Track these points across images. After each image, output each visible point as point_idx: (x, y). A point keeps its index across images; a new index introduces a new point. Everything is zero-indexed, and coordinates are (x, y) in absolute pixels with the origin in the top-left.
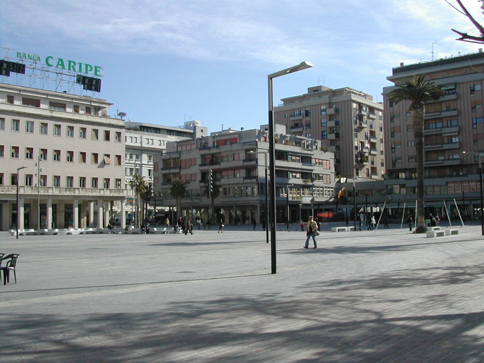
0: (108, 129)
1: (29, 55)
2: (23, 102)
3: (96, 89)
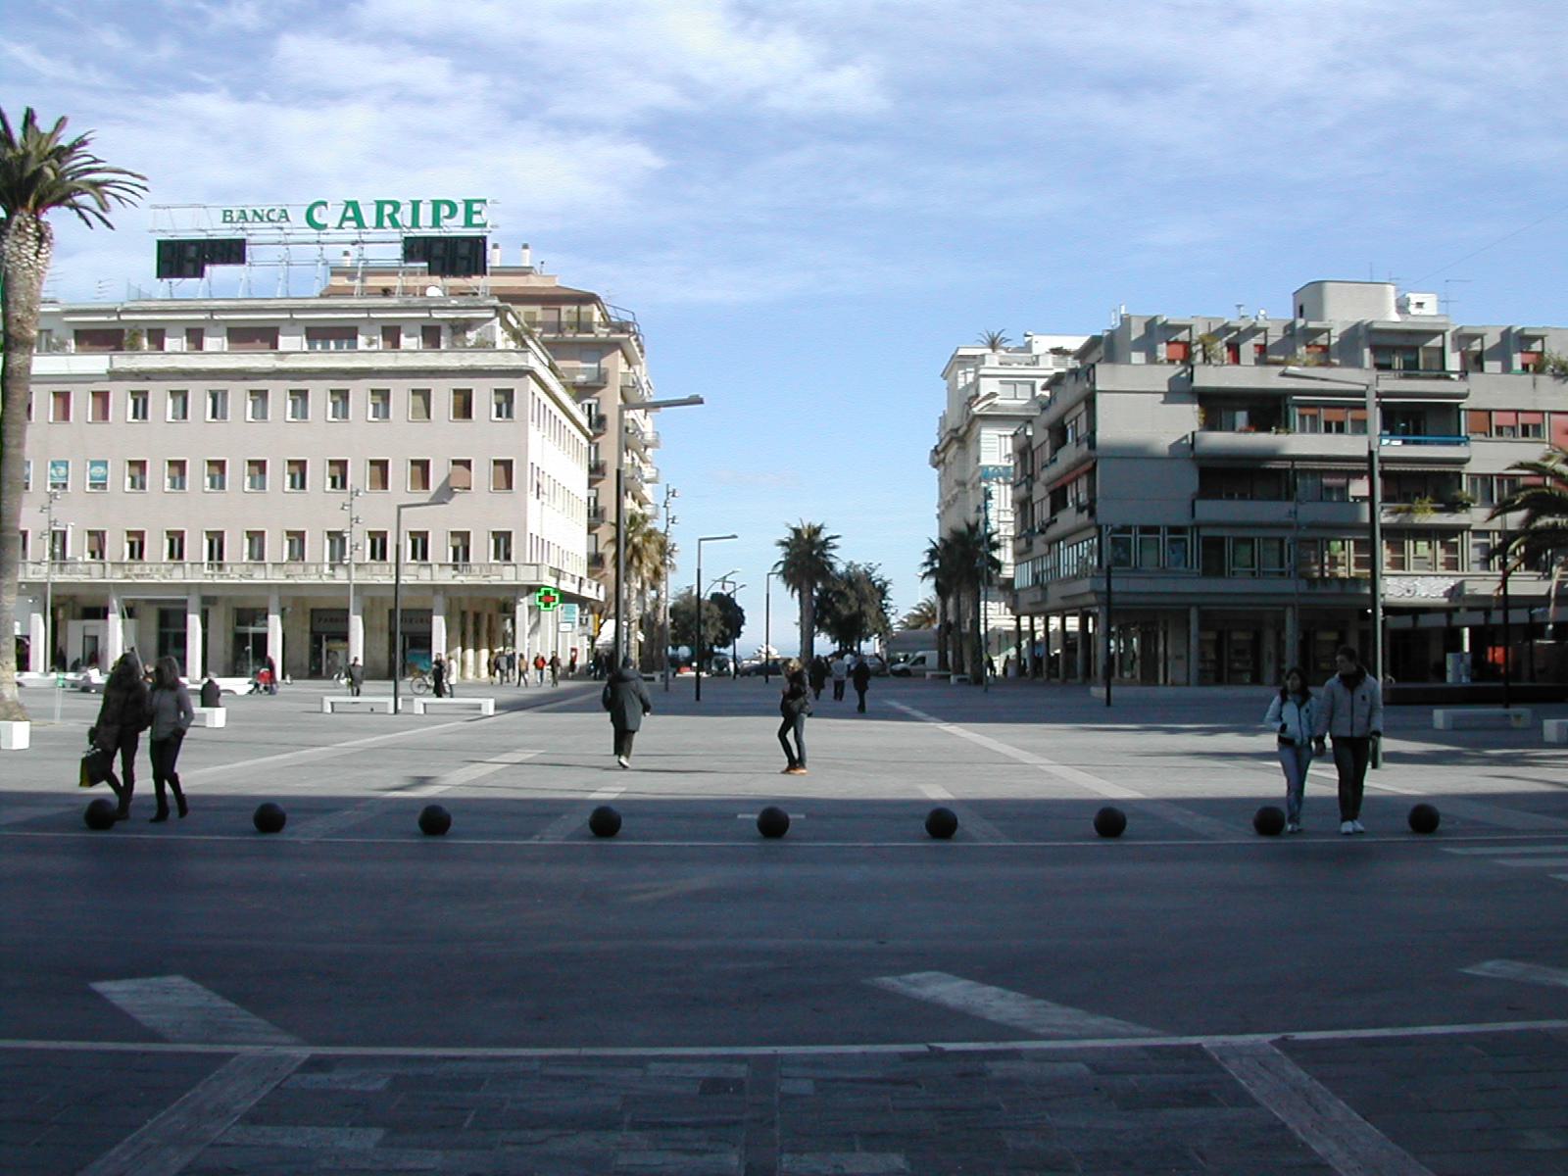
0: (463, 384)
1: (255, 212)
2: (424, 338)
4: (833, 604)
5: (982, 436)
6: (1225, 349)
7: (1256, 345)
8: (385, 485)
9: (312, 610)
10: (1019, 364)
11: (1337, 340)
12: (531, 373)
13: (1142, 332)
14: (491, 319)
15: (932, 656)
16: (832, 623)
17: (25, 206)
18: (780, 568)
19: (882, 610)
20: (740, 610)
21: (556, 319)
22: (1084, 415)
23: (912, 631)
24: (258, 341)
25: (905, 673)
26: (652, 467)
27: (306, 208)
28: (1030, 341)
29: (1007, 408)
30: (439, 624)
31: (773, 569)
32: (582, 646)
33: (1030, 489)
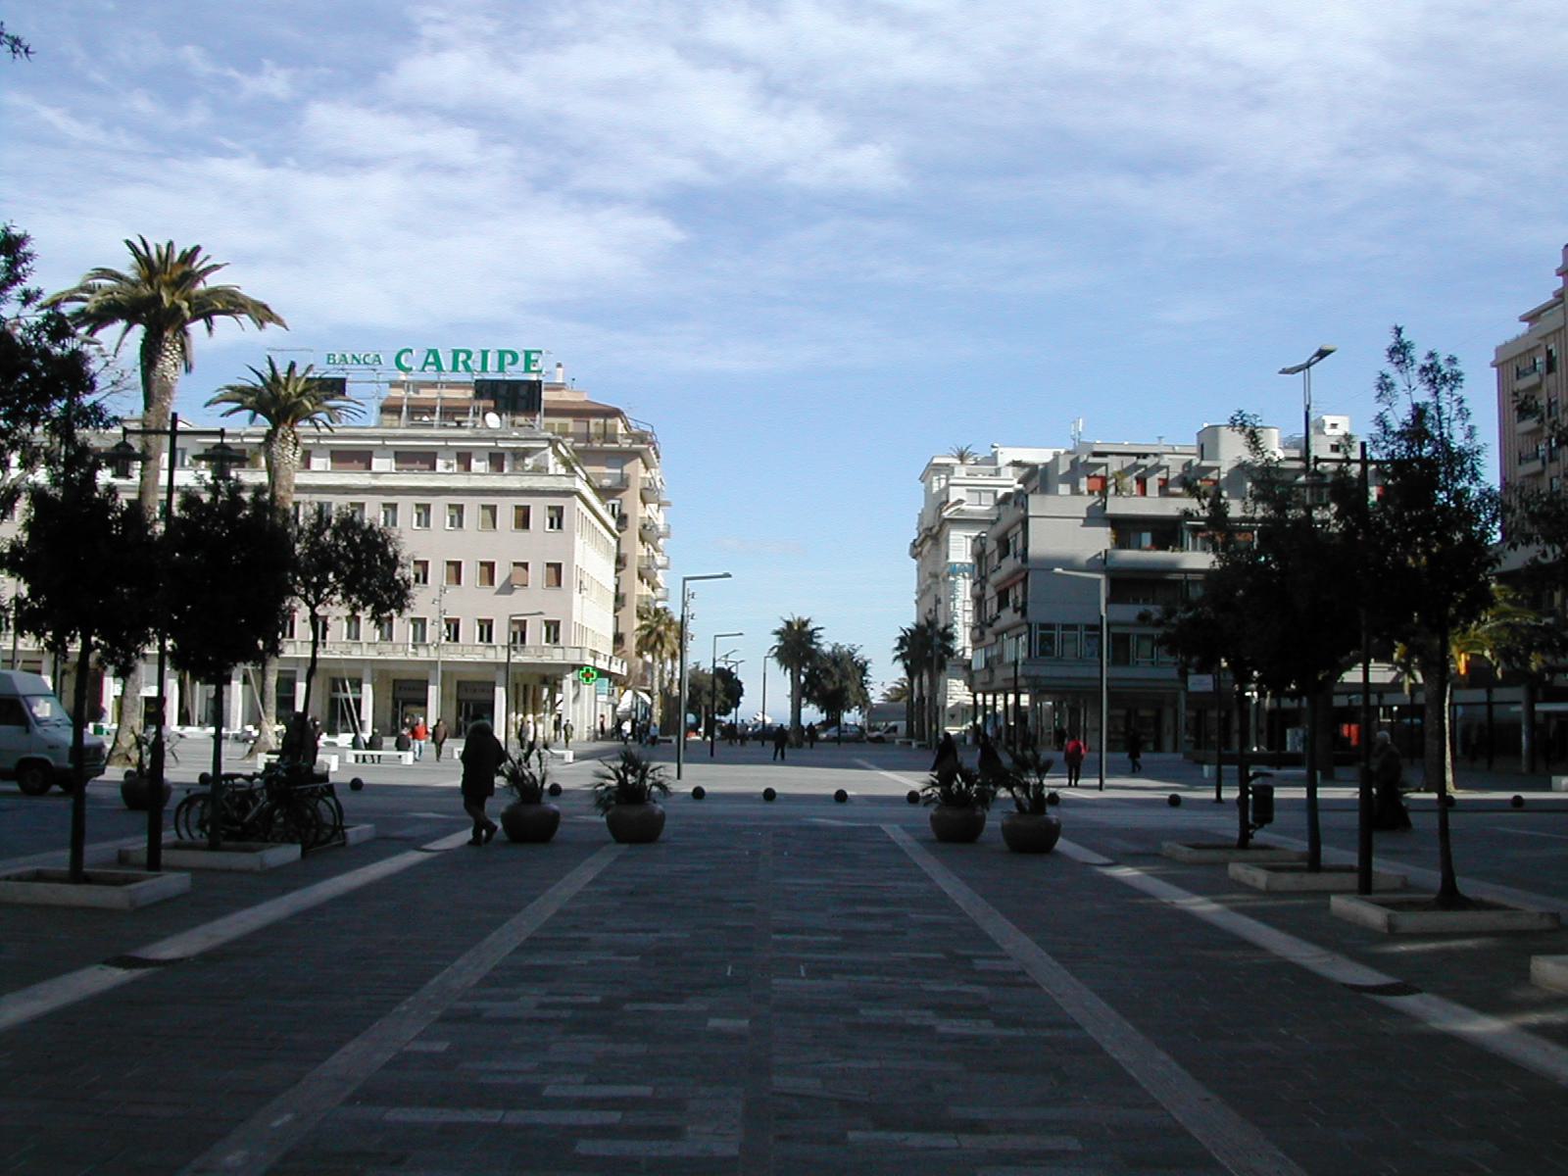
0: (523, 501)
1: (354, 357)
2: (491, 462)
3: (530, 407)
4: (820, 680)
5: (951, 537)
6: (1135, 482)
7: (1160, 479)
8: (458, 582)
9: (395, 681)
10: (984, 475)
11: (1225, 475)
12: (578, 493)
13: (1068, 468)
14: (544, 448)
15: (902, 725)
16: (819, 696)
17: (286, 422)
18: (776, 650)
19: (862, 685)
20: (740, 684)
21: (585, 431)
22: (1021, 533)
23: (894, 704)
24: (356, 462)
25: (879, 740)
26: (663, 555)
27: (395, 354)
28: (996, 452)
29: (973, 513)
30: (500, 693)
31: (769, 653)
32: (608, 713)
33: (983, 588)
